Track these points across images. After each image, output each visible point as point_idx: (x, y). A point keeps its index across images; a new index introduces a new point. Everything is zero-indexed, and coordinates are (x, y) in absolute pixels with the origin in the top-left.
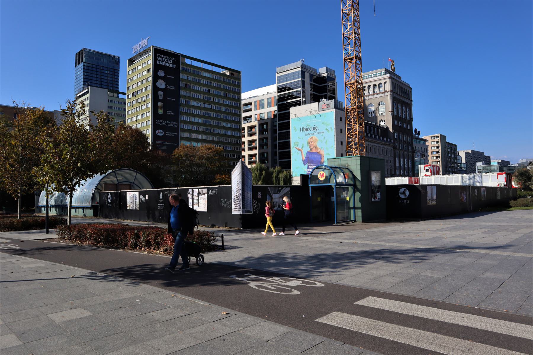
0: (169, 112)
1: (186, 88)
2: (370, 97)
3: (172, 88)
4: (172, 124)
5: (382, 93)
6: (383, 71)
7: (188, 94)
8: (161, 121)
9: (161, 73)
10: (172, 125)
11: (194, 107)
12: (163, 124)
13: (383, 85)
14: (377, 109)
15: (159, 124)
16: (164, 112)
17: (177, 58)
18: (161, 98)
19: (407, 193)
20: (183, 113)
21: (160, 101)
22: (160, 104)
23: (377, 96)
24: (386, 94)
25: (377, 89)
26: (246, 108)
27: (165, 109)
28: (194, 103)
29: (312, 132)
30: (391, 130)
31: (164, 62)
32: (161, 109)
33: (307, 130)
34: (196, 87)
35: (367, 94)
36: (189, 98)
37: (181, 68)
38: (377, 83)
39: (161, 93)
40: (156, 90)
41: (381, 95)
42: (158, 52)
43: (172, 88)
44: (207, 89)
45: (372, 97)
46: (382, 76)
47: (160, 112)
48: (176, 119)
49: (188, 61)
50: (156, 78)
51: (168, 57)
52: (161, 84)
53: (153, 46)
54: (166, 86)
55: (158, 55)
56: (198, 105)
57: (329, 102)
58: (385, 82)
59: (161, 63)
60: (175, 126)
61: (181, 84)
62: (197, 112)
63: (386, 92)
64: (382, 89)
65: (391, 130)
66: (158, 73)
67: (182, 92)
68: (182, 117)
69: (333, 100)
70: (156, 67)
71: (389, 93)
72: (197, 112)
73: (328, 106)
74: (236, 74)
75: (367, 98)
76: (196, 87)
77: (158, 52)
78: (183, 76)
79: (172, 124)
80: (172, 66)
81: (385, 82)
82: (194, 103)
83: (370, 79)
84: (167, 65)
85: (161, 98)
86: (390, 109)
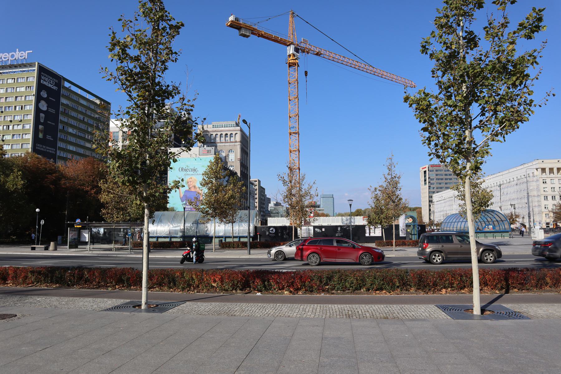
0: (49, 137)
1: (66, 114)
2: (221, 144)
3: (53, 111)
4: (51, 150)
5: (232, 142)
6: (234, 123)
7: (65, 120)
8: (41, 146)
9: (44, 94)
10: (51, 151)
11: (71, 134)
12: (42, 149)
13: (234, 135)
14: (228, 155)
15: (39, 148)
16: (44, 136)
17: (59, 79)
18: (42, 121)
19: (274, 231)
20: (62, 140)
21: (42, 124)
22: (41, 127)
23: (228, 144)
24: (236, 144)
25: (228, 139)
26: (451, 199)
27: (45, 133)
28: (70, 130)
29: (192, 173)
30: (239, 175)
31: (49, 83)
32: (42, 133)
33: (186, 170)
34: (73, 114)
35: (219, 141)
36: (67, 124)
37: (63, 91)
38: (229, 133)
39: (42, 115)
40: (38, 111)
41: (231, 144)
42: (43, 71)
43: (53, 111)
44: (82, 117)
45: (224, 144)
46: (234, 128)
47: (41, 136)
48: (54, 144)
49: (67, 85)
50: (39, 98)
51: (51, 78)
52: (43, 106)
53: (38, 63)
54: (48, 109)
55: (42, 73)
56: (74, 133)
57: (209, 148)
58: (236, 134)
59: (45, 83)
60: (53, 152)
61: (61, 109)
62: (73, 139)
63: (236, 142)
64: (233, 139)
65: (239, 175)
66: (42, 93)
67: (61, 118)
68: (60, 144)
69: (214, 148)
70: (40, 87)
71: (239, 143)
72: (73, 139)
73: (209, 152)
74: (106, 104)
75: (218, 145)
76: (73, 114)
77: (43, 71)
78: (63, 101)
79: (51, 150)
80: (55, 88)
81: (236, 134)
82: (70, 130)
83: (223, 128)
84: (50, 85)
85: (42, 121)
86: (239, 156)
